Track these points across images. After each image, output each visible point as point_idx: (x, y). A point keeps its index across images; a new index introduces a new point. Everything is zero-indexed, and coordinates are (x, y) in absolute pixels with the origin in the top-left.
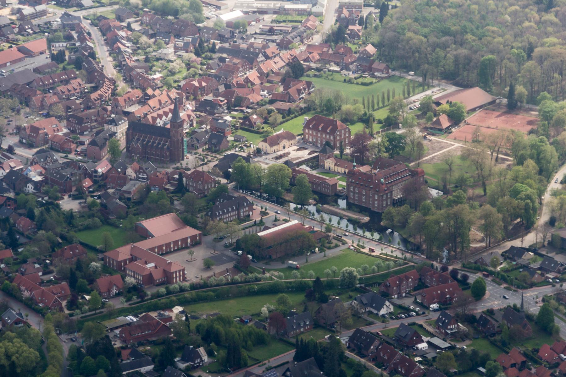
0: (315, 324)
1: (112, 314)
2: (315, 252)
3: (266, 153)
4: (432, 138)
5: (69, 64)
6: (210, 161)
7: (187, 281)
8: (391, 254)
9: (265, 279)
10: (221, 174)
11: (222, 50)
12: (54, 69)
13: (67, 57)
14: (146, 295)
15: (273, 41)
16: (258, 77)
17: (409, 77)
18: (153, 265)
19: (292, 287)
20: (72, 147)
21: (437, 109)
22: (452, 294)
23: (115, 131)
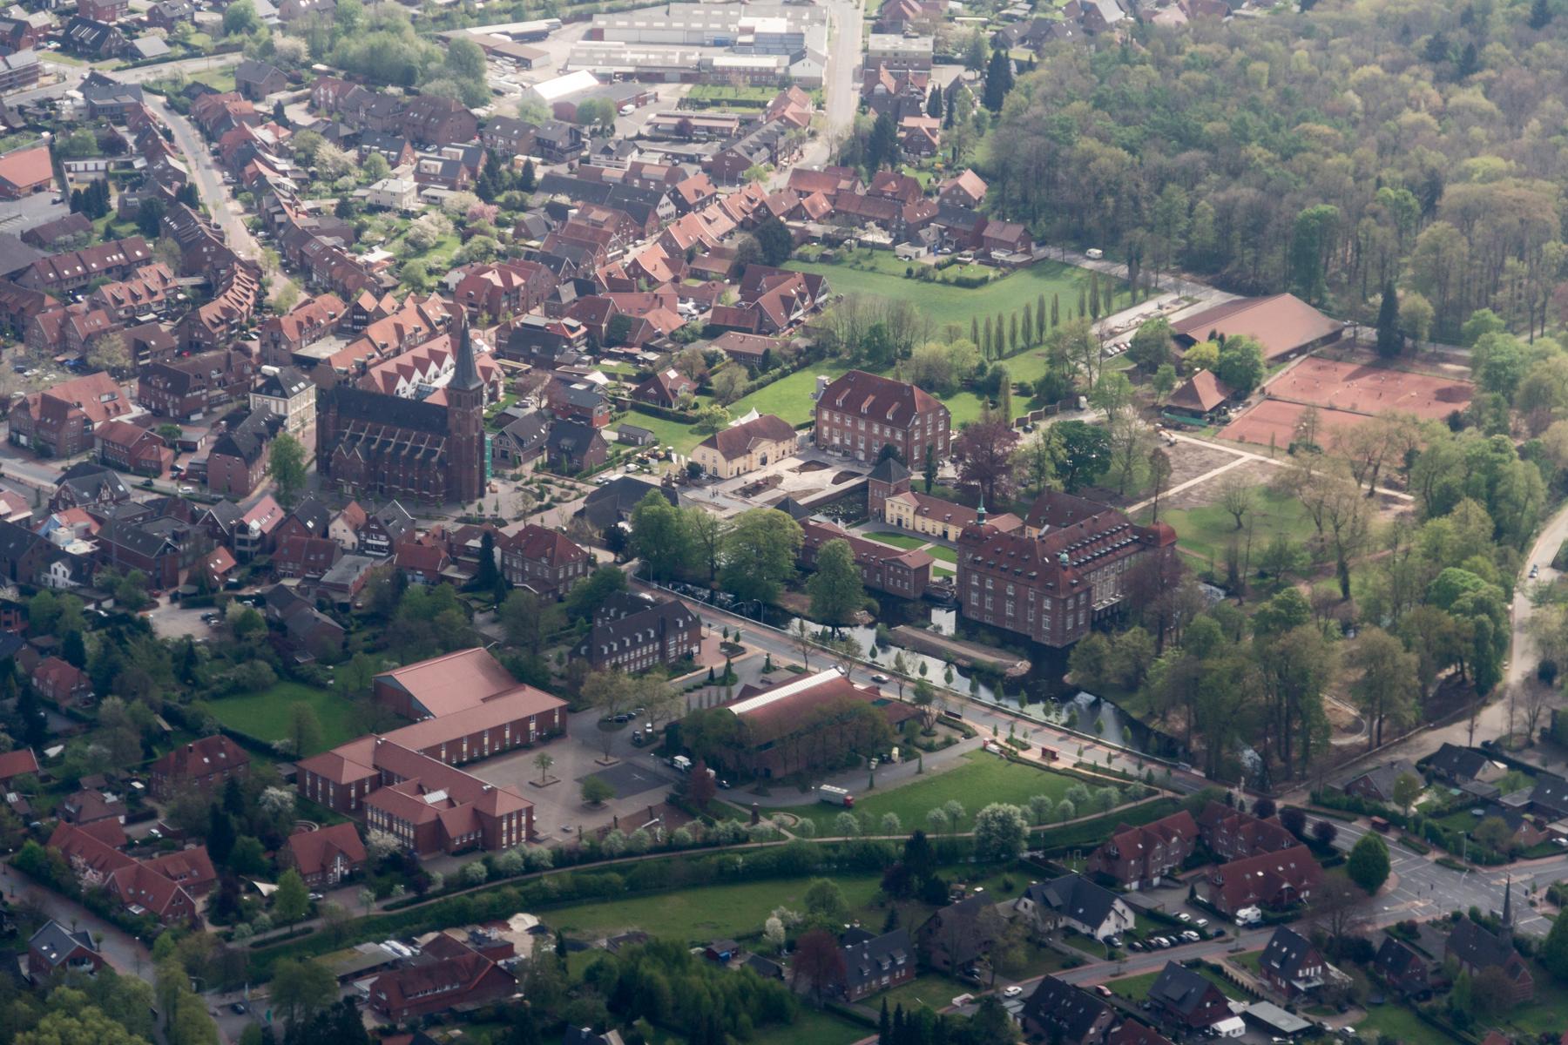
0: (919, 965)
1: (341, 936)
2: (890, 760)
3: (715, 479)
4: (1176, 436)
5: (120, 220)
6: (559, 500)
7: (539, 842)
8: (1106, 766)
9: (762, 836)
10: (596, 535)
11: (552, 184)
12: (81, 234)
13: (114, 202)
14: (429, 881)
15: (691, 159)
16: (664, 260)
17: (1089, 265)
18: (441, 795)
19: (841, 860)
20: (163, 458)
21: (1186, 354)
22: (1296, 878)
23: (281, 412)
